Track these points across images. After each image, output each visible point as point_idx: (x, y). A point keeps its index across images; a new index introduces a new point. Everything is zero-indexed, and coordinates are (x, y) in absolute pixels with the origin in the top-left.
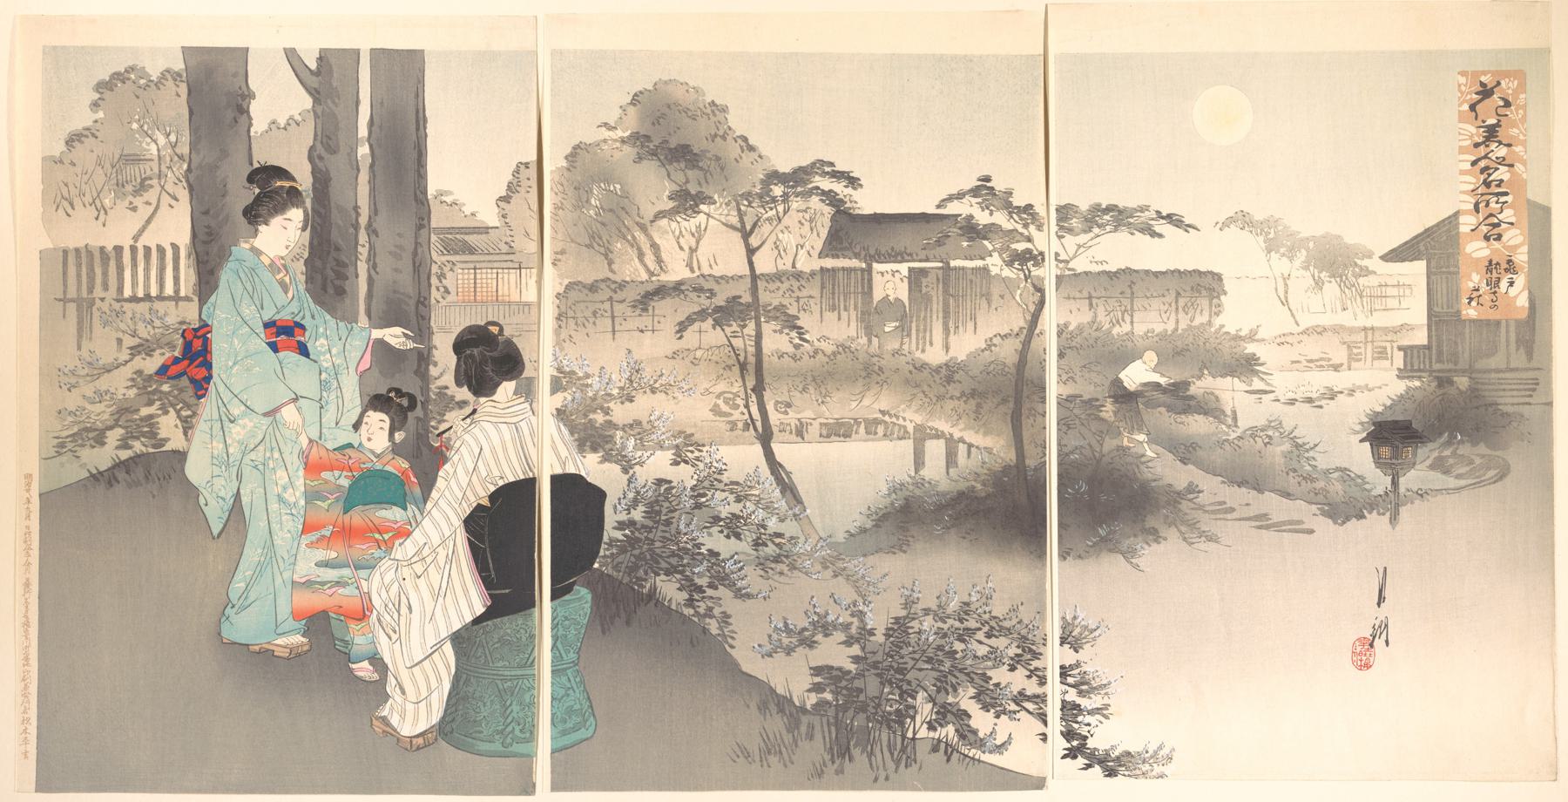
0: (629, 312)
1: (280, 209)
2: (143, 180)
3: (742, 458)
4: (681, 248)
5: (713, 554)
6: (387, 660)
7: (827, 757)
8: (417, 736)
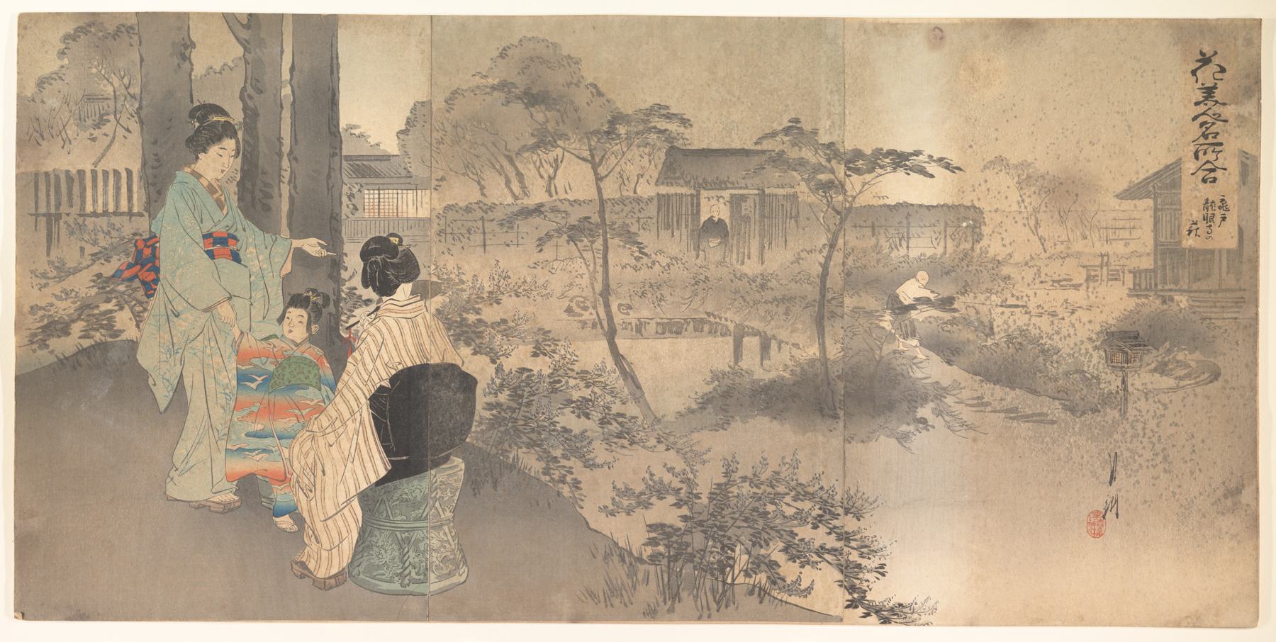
0: (497, 229)
1: (219, 139)
2: (101, 116)
3: (593, 353)
4: (542, 177)
5: (565, 430)
6: (306, 515)
7: (661, 600)
8: (330, 578)
